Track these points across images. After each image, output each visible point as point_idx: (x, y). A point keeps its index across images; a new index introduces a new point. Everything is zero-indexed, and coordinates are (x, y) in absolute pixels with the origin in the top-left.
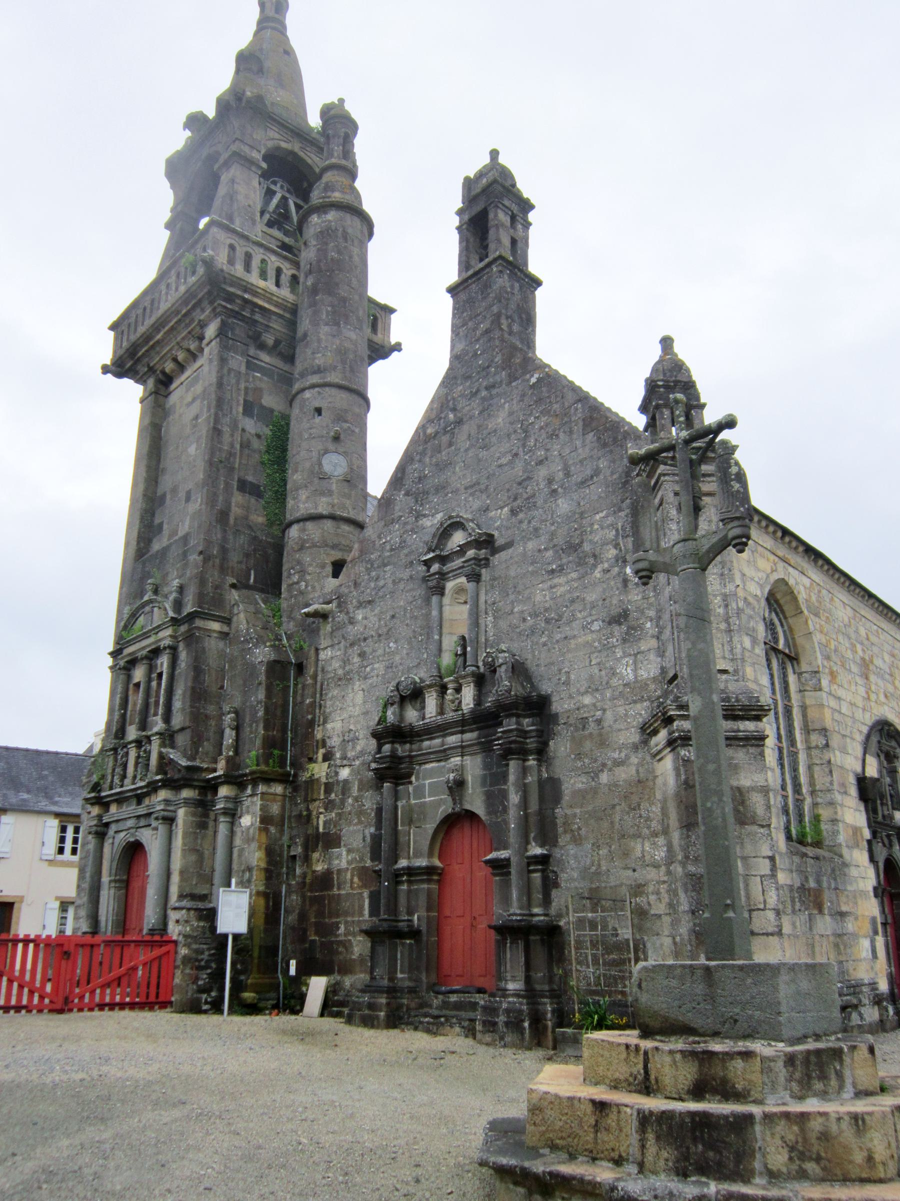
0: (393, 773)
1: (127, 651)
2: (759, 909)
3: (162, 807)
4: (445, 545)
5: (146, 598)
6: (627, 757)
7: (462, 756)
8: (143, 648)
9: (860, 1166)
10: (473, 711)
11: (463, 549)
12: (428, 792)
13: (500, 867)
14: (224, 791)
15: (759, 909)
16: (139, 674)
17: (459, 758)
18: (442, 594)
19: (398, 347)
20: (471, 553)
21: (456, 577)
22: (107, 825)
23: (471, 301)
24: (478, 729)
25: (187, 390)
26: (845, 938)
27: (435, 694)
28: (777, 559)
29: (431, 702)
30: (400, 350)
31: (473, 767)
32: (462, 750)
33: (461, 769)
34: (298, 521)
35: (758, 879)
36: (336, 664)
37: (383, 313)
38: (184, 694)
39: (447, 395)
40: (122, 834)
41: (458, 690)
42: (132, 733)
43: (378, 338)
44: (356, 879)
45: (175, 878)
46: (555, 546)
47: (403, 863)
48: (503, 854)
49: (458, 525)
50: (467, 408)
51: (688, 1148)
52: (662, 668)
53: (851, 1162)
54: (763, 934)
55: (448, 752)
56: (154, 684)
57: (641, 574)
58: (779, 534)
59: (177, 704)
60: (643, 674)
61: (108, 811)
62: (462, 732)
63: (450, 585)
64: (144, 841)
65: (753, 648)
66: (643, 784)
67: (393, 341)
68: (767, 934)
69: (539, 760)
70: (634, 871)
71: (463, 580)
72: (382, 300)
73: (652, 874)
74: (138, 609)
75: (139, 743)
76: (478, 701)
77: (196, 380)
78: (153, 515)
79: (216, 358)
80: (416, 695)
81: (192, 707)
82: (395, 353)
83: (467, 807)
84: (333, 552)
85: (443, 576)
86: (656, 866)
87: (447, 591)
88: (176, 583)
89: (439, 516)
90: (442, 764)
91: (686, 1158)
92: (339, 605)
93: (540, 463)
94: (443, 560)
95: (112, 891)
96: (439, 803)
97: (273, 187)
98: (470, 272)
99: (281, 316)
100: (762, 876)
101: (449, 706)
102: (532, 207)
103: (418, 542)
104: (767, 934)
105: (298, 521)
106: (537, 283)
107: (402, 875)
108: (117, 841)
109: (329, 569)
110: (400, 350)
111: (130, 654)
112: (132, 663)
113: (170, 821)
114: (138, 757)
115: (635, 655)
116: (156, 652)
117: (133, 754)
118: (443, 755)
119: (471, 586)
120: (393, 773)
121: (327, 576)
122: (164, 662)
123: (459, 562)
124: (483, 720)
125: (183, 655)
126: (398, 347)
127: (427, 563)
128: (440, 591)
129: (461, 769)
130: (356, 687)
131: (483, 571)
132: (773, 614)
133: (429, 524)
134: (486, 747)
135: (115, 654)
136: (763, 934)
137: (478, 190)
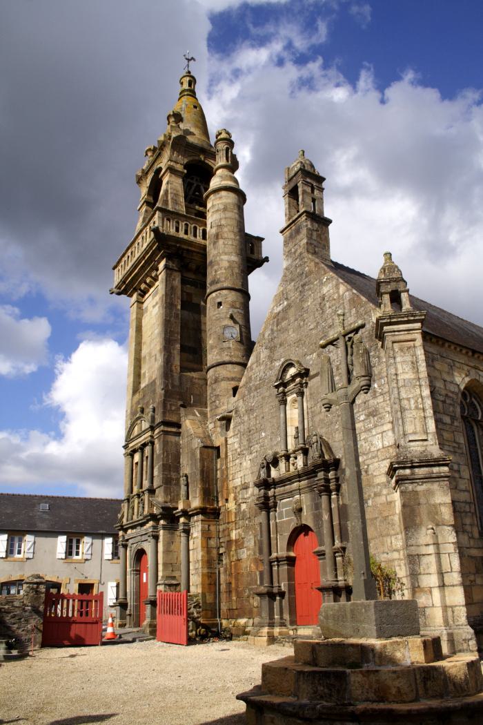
0: (267, 505)
1: (131, 445)
2: (448, 572)
3: (151, 530)
4: (285, 376)
5: (138, 416)
6: (381, 491)
7: (300, 494)
8: (137, 444)
9: (394, 695)
10: (303, 468)
11: (294, 378)
12: (284, 517)
13: (321, 554)
14: (182, 520)
15: (448, 572)
16: (137, 457)
17: (298, 496)
18: (285, 404)
19: (267, 259)
20: (298, 380)
21: (292, 394)
22: (127, 540)
23: (291, 237)
24: (308, 479)
25: (153, 298)
26: (263, 589)
27: (284, 461)
28: (469, 368)
29: (282, 464)
30: (268, 261)
31: (305, 500)
32: (299, 490)
33: (300, 501)
34: (213, 367)
35: (447, 555)
36: (236, 446)
37: (256, 241)
38: (159, 468)
39: (282, 291)
40: (135, 545)
41: (296, 458)
42: (136, 490)
43: (255, 256)
44: (252, 565)
45: (160, 567)
46: (340, 374)
47: (274, 555)
48: (322, 548)
49: (291, 365)
50: (293, 298)
51: (317, 688)
52: (395, 440)
53: (390, 693)
54: (451, 586)
55: (293, 492)
56: (145, 463)
57: (325, 406)
58: (470, 354)
59: (156, 473)
60: (386, 443)
61: (126, 533)
62: (300, 481)
63: (289, 399)
64: (145, 549)
65: (453, 422)
66: (390, 503)
67: (264, 256)
68: (453, 586)
69: (337, 495)
70: (388, 554)
71: (295, 395)
72: (255, 234)
73: (396, 555)
74: (134, 423)
75: (138, 496)
76: (305, 464)
77: (157, 293)
78: (140, 368)
79: (164, 281)
80: (275, 462)
81: (163, 474)
82: (266, 263)
83: (304, 522)
84: (232, 382)
85: (284, 394)
86: (397, 551)
87: (288, 402)
88: (151, 407)
89: (282, 360)
90: (291, 499)
91: (315, 692)
92: (236, 413)
93: (330, 327)
94: (285, 385)
95: (132, 576)
96: (289, 522)
97: (191, 181)
98: (291, 221)
99: (198, 253)
100: (449, 554)
101: (292, 468)
102: (324, 179)
103: (273, 374)
104: (453, 586)
105: (213, 367)
106: (329, 222)
107: (274, 562)
108: (133, 548)
109: (231, 392)
110: (268, 261)
111: (132, 447)
112: (134, 451)
113: (156, 538)
114: (139, 503)
115: (382, 433)
116: (144, 445)
117: (136, 501)
118: (291, 494)
119: (299, 398)
120: (267, 505)
121: (230, 396)
122: (147, 450)
123: (292, 386)
124: (309, 473)
125: (157, 446)
126: (267, 259)
127: (277, 387)
128: (284, 402)
129: (300, 501)
130: (247, 458)
131: (305, 390)
132: (473, 399)
133: (277, 364)
134: (310, 488)
135: (125, 447)
136: (451, 586)
137: (293, 174)
